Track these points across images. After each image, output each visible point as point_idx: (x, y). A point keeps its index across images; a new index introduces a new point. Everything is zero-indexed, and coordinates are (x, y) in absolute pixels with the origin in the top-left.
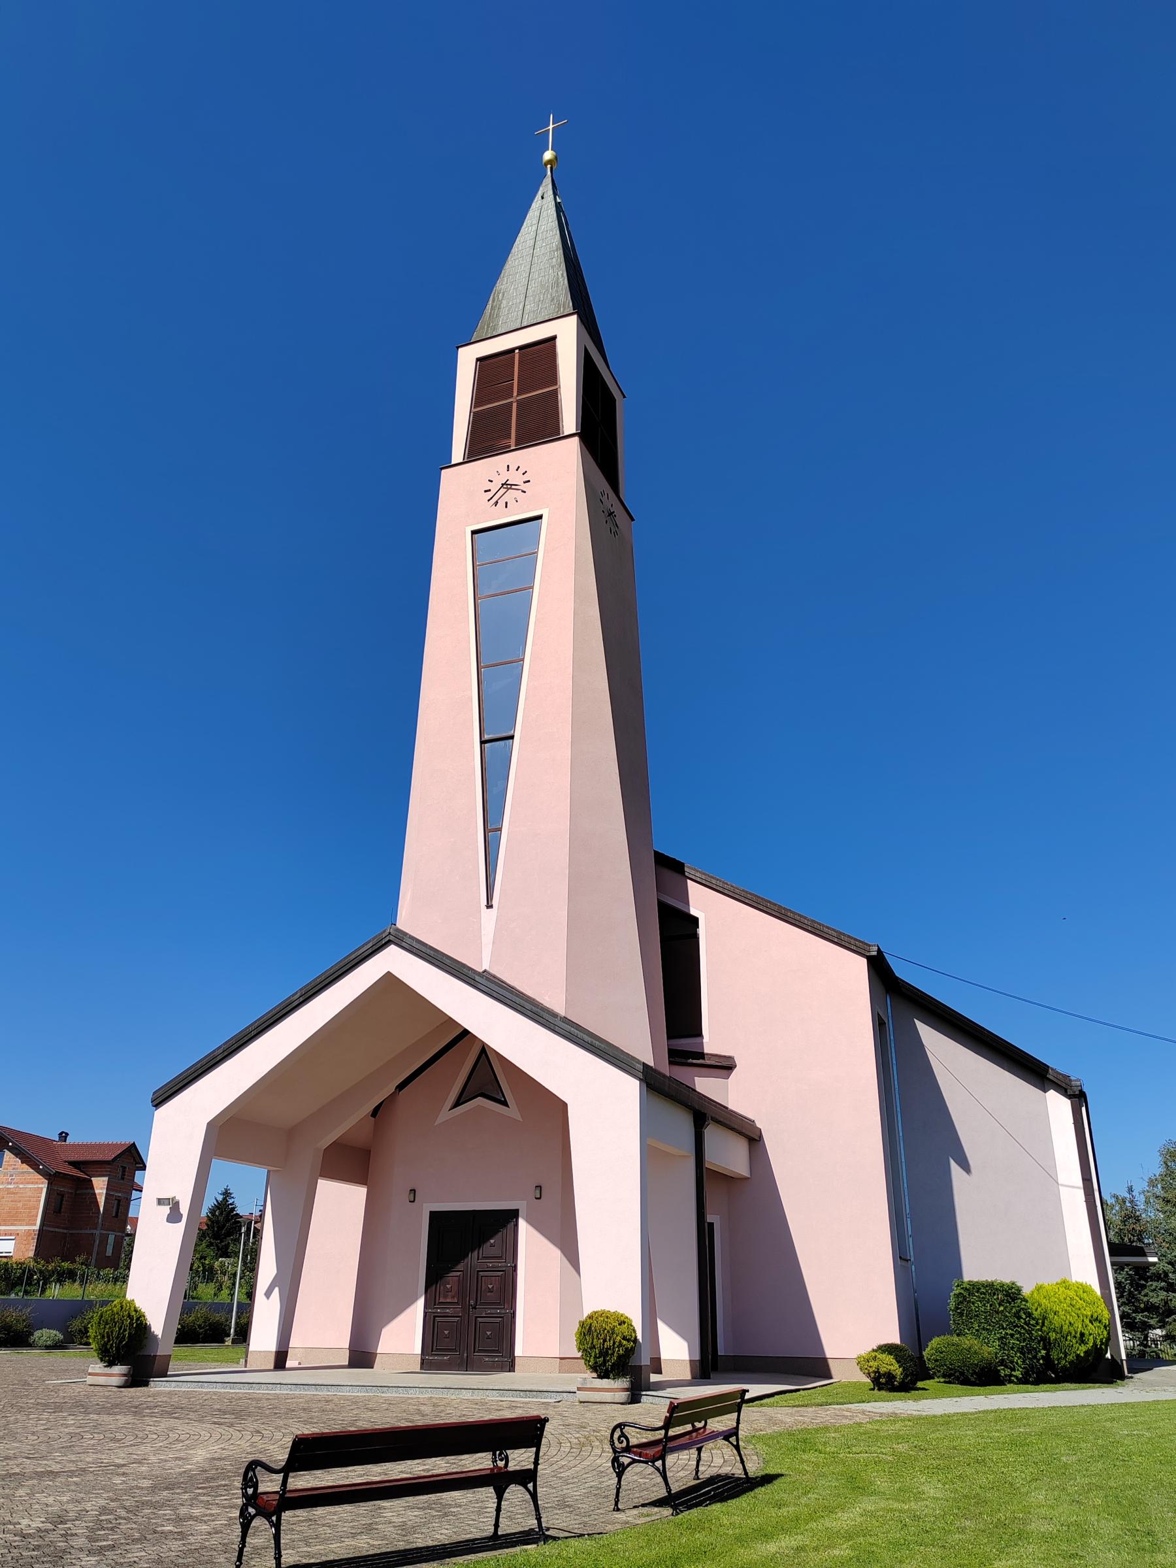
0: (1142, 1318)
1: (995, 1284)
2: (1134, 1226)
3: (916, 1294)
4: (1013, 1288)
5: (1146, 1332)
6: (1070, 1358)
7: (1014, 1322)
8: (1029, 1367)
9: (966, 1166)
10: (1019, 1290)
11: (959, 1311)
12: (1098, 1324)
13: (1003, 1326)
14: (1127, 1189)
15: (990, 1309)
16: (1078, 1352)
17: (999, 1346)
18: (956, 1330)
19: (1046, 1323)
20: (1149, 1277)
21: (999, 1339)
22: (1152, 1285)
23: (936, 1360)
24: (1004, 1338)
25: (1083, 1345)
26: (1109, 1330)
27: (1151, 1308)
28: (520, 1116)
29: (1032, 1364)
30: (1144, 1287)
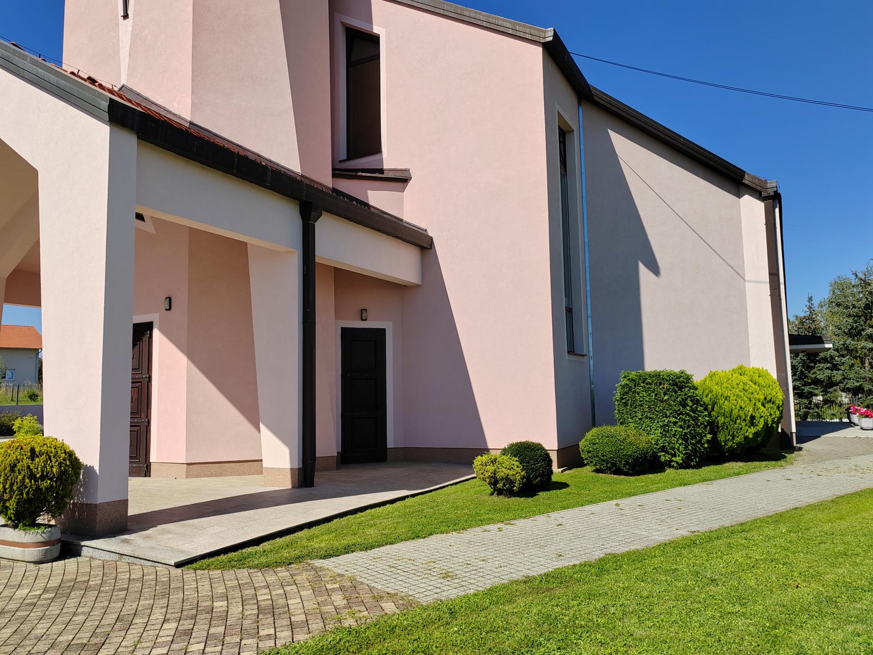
0: (809, 390)
1: (661, 374)
2: (810, 325)
3: (593, 386)
4: (681, 376)
5: (811, 399)
6: (737, 440)
7: (679, 410)
8: (691, 451)
9: (655, 270)
10: (688, 379)
11: (624, 401)
12: (771, 405)
13: (666, 414)
14: (807, 299)
15: (655, 399)
16: (747, 434)
17: (661, 433)
18: (620, 419)
19: (716, 408)
20: (817, 361)
21: (661, 427)
22: (819, 366)
23: (589, 452)
24: (667, 425)
25: (752, 427)
26: (782, 410)
27: (816, 382)
28: (154, 229)
29: (695, 449)
30: (813, 367)
